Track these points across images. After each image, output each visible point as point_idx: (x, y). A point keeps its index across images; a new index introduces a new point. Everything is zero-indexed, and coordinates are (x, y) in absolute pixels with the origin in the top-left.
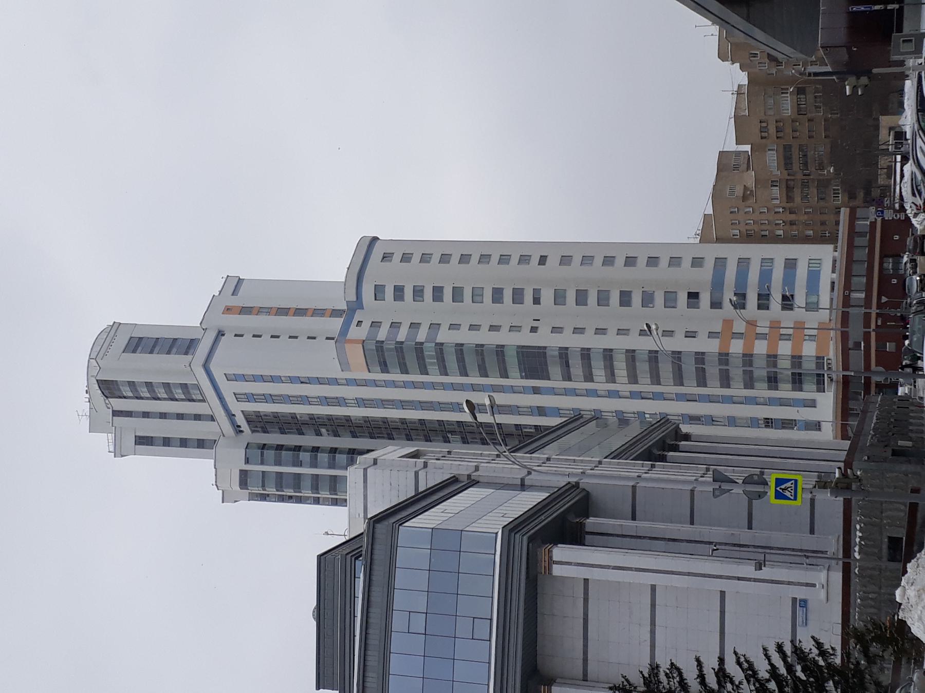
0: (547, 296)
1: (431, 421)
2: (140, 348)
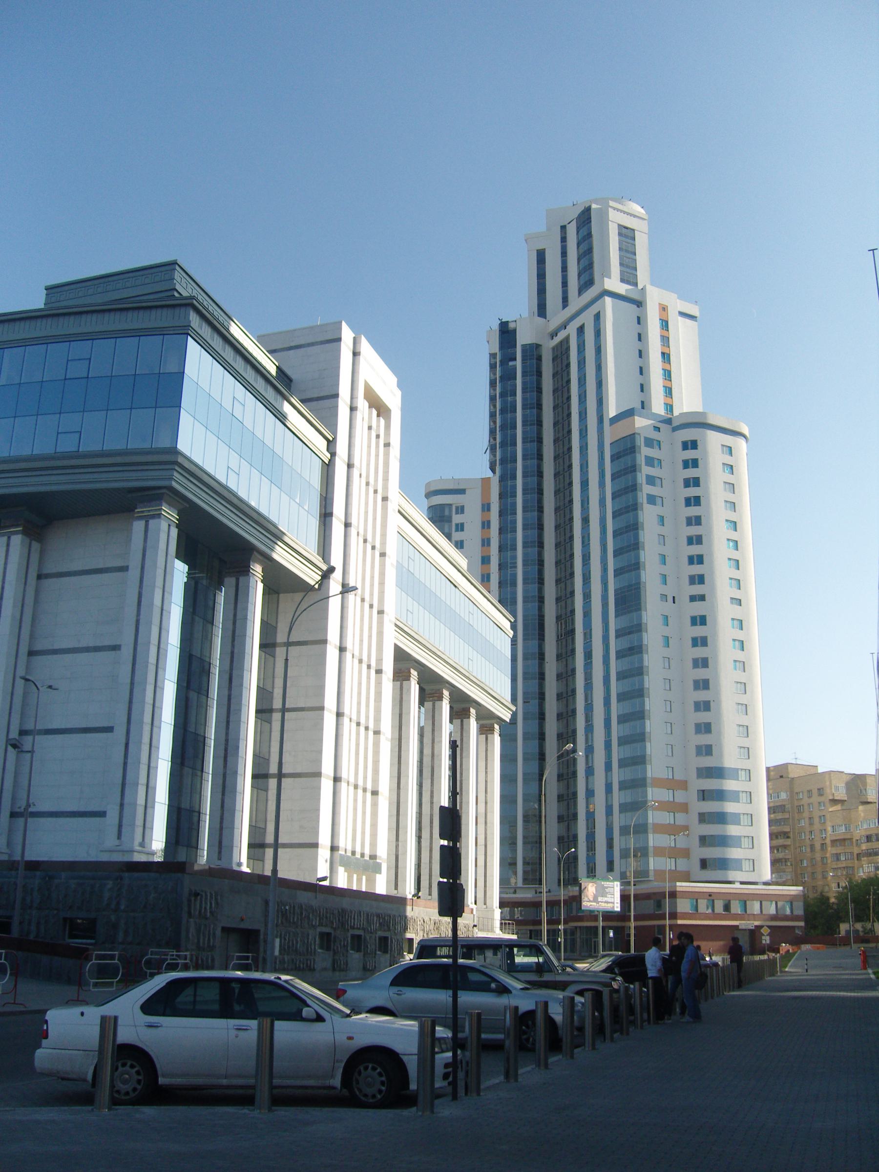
0: (698, 609)
1: (575, 786)
2: (624, 239)
